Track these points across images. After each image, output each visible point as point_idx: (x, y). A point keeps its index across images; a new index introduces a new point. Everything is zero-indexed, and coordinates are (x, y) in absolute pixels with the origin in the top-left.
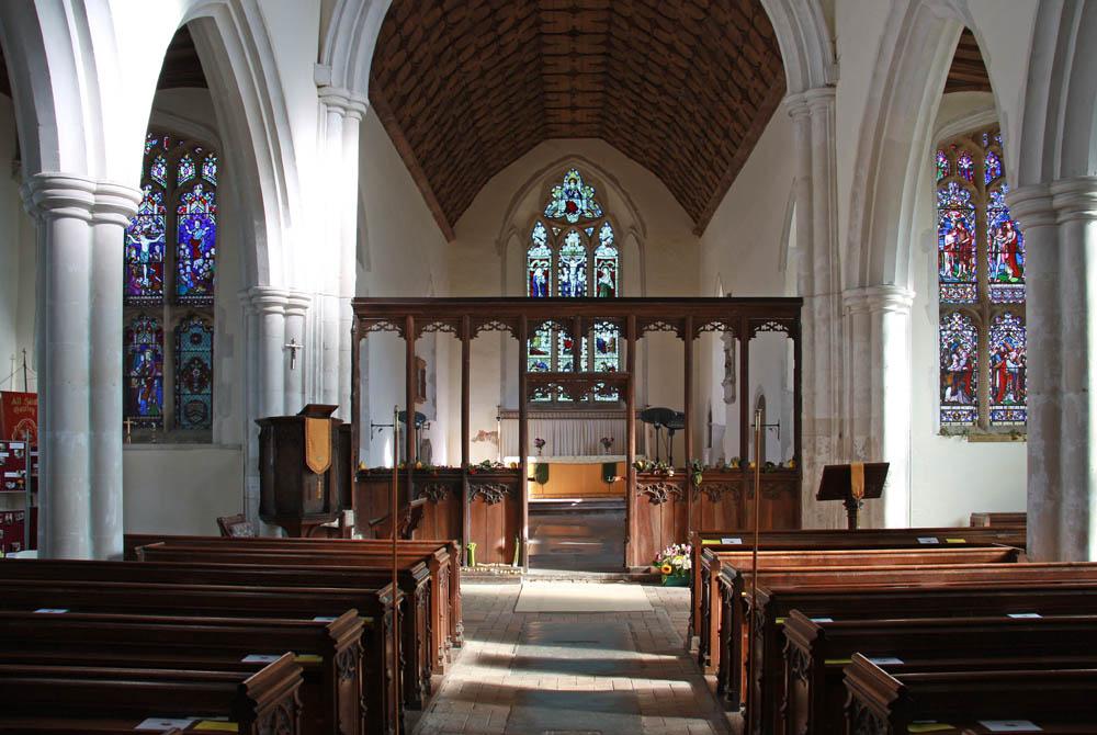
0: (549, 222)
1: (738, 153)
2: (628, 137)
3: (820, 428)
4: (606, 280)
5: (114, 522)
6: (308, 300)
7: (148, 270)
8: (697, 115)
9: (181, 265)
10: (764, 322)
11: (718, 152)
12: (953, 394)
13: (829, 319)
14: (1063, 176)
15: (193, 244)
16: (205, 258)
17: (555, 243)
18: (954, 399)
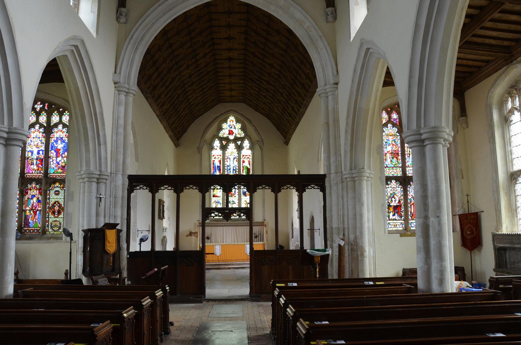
0: (221, 139)
1: (301, 110)
2: (255, 102)
3: (335, 231)
4: (246, 164)
5: (9, 280)
6: (108, 176)
7: (37, 162)
8: (284, 94)
9: (51, 160)
10: (309, 185)
11: (293, 110)
12: (394, 215)
13: (337, 184)
14: (425, 126)
15: (57, 151)
16: (62, 157)
17: (224, 148)
18: (394, 217)
